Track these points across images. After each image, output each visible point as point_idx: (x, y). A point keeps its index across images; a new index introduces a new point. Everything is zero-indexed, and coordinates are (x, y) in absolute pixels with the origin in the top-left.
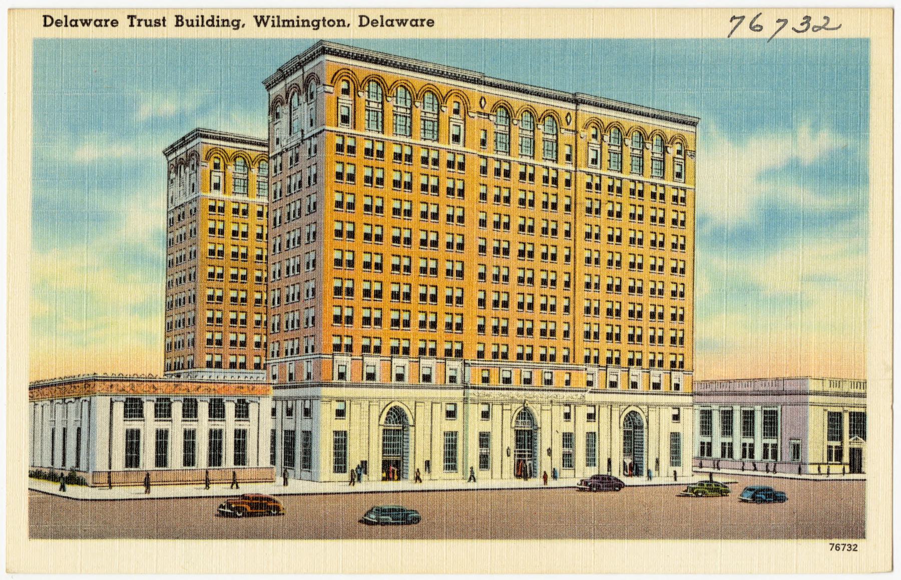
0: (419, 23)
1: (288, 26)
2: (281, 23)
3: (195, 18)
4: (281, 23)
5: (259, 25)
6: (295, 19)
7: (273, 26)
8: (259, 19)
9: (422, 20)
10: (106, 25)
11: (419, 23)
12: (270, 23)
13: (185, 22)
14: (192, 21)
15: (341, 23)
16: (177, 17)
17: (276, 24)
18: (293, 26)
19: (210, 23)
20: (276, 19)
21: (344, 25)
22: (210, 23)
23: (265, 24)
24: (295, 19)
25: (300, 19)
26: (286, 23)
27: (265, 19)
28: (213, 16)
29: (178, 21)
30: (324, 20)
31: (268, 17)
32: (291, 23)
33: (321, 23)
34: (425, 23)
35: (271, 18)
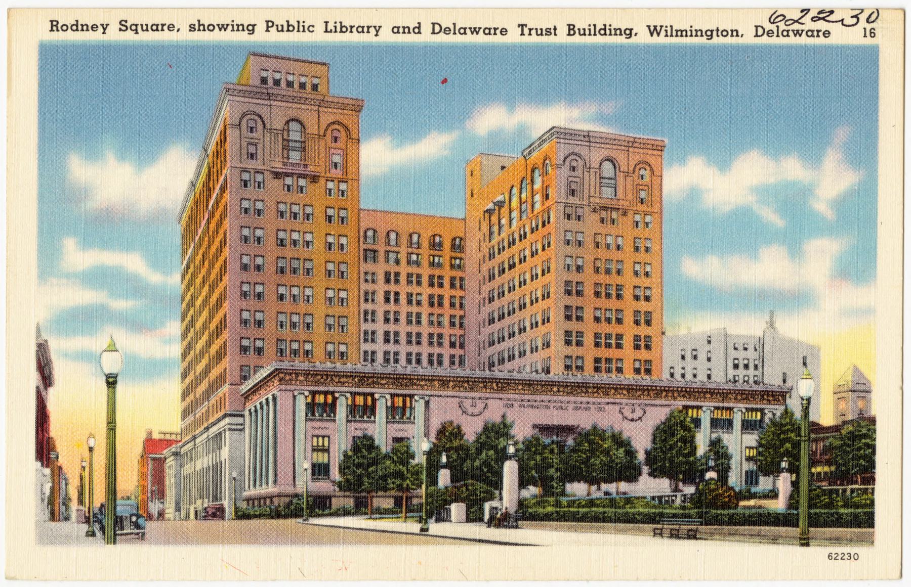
0: (492, 31)
1: (682, 36)
2: (674, 33)
3: (587, 28)
4: (674, 33)
5: (652, 35)
6: (688, 29)
7: (666, 36)
8: (652, 28)
9: (163, 25)
10: (495, 34)
11: (492, 31)
12: (663, 33)
13: (411, 31)
14: (584, 30)
15: (735, 33)
16: (52, 21)
17: (669, 34)
18: (686, 36)
19: (74, 28)
20: (669, 29)
21: (737, 35)
22: (74, 28)
23: (658, 34)
24: (688, 29)
25: (693, 29)
26: (679, 33)
27: (658, 29)
28: (77, 21)
29: (569, 30)
30: (718, 30)
31: (661, 27)
32: (684, 33)
33: (715, 33)
34: (498, 32)
35: (664, 28)
